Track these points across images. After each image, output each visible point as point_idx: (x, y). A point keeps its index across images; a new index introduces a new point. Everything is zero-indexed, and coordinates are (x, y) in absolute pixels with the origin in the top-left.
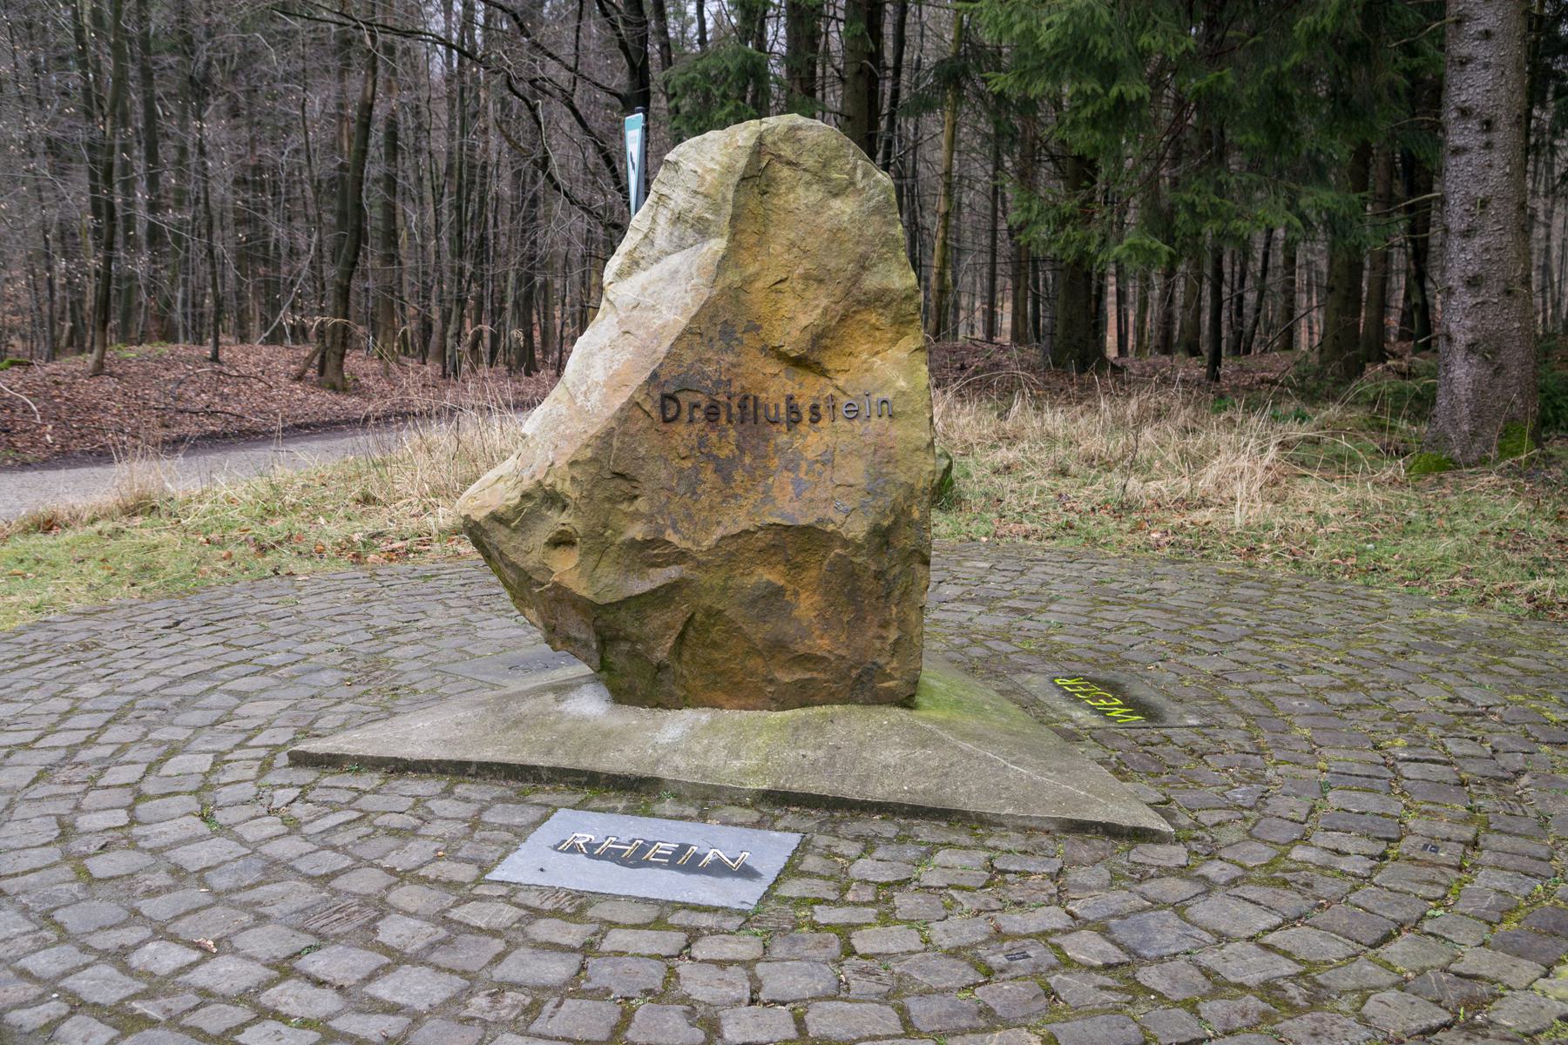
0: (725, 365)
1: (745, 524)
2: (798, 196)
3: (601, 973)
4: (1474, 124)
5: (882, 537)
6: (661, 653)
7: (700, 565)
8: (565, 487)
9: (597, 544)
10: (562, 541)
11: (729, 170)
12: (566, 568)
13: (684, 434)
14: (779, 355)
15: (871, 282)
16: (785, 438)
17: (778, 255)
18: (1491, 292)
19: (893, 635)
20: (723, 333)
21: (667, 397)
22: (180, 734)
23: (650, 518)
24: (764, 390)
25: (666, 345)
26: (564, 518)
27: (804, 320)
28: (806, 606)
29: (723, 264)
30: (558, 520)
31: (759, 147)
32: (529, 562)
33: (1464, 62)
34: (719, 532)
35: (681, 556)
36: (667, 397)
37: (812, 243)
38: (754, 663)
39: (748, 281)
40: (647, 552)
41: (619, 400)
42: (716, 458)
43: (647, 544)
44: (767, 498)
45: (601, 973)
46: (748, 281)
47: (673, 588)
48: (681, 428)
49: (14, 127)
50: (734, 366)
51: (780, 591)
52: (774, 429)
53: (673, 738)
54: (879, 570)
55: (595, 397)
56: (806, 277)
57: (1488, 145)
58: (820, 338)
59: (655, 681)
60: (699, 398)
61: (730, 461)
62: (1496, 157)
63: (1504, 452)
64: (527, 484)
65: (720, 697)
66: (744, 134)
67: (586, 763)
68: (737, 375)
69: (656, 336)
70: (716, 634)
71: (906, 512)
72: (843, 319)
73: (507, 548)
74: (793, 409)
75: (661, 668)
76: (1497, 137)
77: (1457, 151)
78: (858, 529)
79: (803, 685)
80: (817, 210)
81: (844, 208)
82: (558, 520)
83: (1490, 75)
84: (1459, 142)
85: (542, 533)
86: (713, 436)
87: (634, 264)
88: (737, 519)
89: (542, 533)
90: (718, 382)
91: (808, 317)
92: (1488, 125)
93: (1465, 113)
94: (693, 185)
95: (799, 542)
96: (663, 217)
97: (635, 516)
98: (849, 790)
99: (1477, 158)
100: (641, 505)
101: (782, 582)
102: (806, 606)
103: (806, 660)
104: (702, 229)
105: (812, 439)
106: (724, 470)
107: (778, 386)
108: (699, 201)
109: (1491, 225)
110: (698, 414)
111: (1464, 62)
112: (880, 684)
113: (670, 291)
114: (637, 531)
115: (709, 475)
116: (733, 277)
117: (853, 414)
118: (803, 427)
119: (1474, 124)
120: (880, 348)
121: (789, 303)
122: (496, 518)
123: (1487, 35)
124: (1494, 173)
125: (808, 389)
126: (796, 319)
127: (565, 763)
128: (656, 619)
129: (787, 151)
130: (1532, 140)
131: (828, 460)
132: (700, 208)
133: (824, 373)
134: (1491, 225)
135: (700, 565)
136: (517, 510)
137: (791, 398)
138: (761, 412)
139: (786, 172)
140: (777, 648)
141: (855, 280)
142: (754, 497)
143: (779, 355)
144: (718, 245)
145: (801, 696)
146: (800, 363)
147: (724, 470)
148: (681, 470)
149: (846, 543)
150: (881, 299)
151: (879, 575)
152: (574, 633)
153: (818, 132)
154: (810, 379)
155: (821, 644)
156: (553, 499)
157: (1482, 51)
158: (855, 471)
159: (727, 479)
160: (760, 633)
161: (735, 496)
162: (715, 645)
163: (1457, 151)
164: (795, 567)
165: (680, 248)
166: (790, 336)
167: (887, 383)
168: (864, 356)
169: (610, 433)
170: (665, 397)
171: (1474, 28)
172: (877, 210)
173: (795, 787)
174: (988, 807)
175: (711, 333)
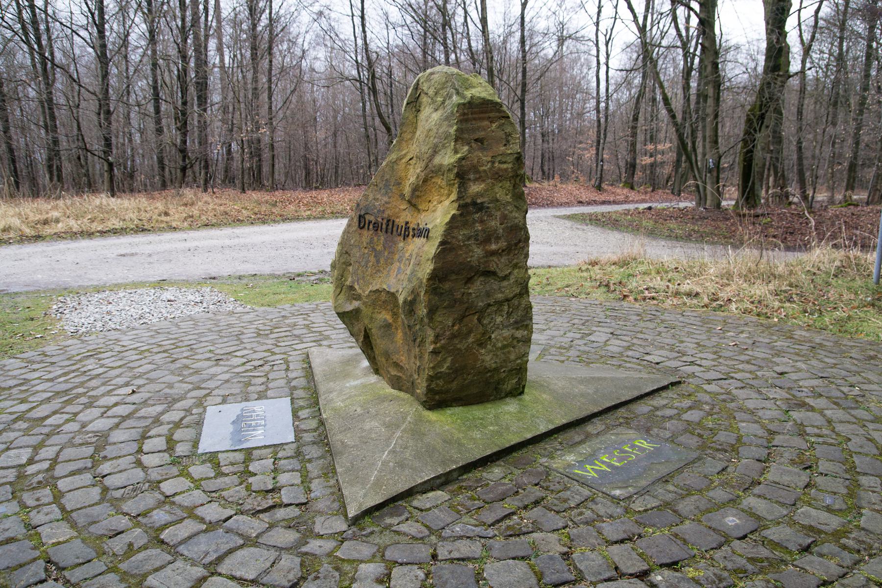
0: (383, 202)
3: (46, 494)
13: (367, 234)
15: (437, 160)
16: (401, 244)
20: (385, 185)
22: (659, 490)
24: (398, 217)
42: (375, 250)
45: (46, 494)
49: (541, 19)
50: (386, 203)
52: (399, 238)
60: (372, 218)
61: (380, 252)
68: (387, 208)
72: (425, 181)
74: (407, 229)
86: (375, 238)
90: (379, 211)
101: (391, 321)
110: (371, 227)
115: (372, 259)
118: (410, 239)
120: (443, 199)
137: (407, 223)
138: (395, 229)
141: (431, 158)
148: (364, 254)
159: (378, 261)
161: (379, 271)
168: (435, 203)
170: (360, 216)
175: (381, 185)
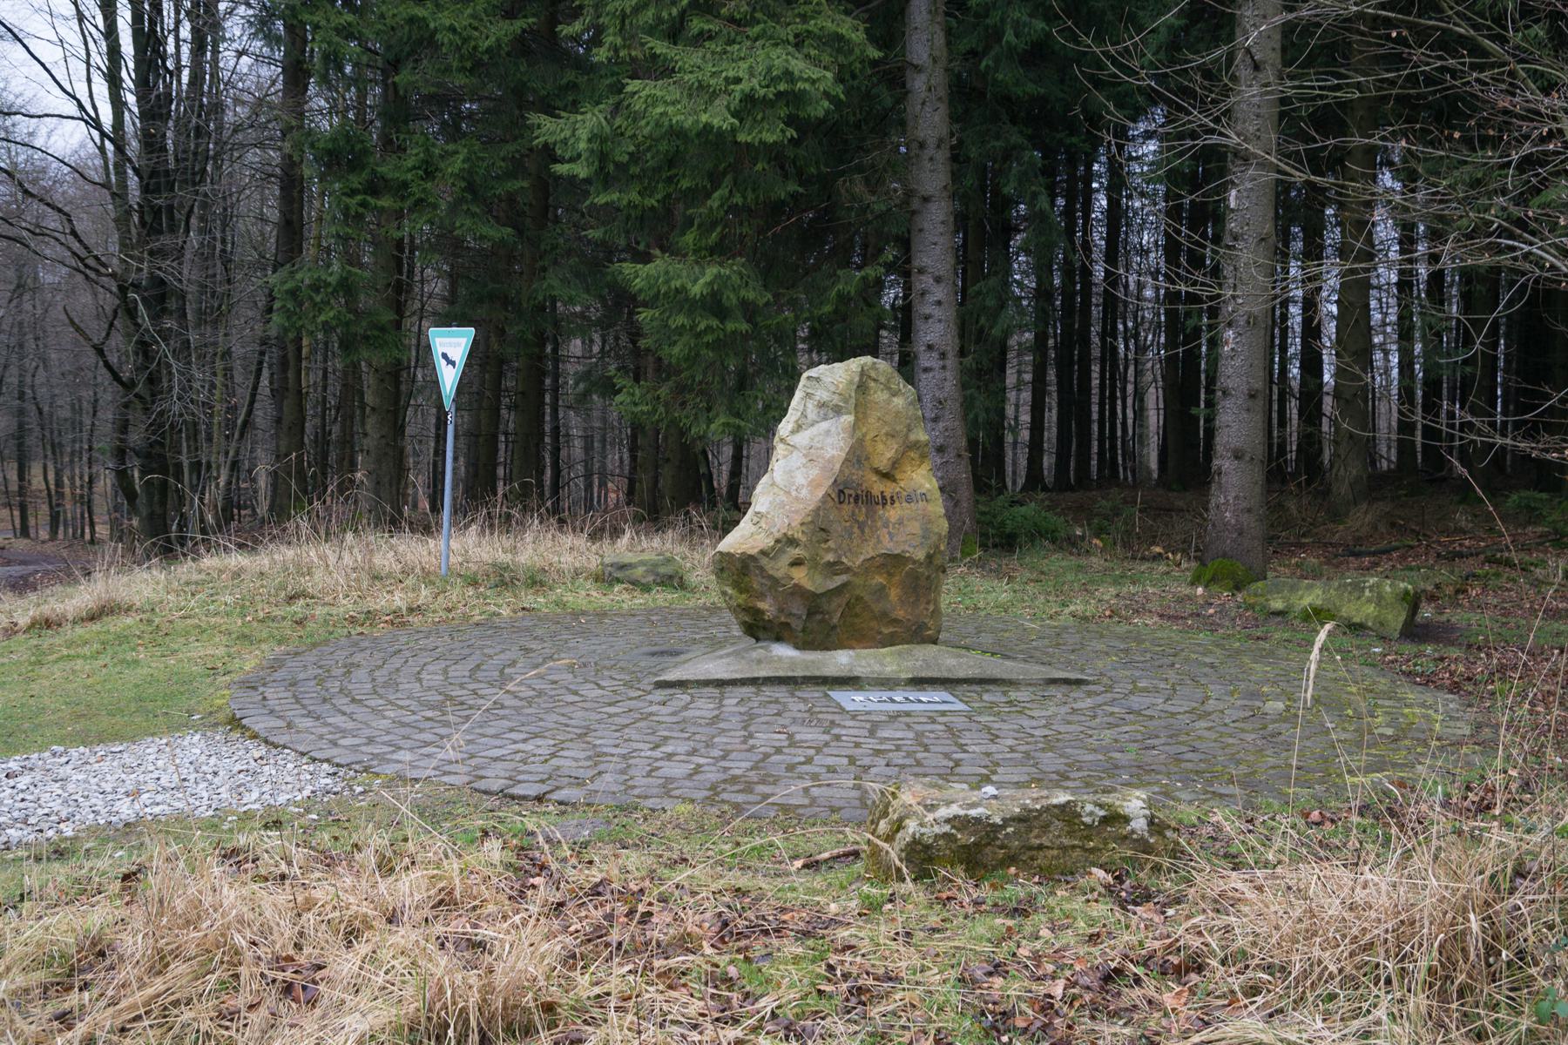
1: (872, 554)
2: (880, 396)
4: (935, 355)
5: (929, 557)
6: (835, 621)
7: (855, 574)
8: (798, 535)
9: (814, 564)
10: (797, 563)
11: (851, 382)
12: (800, 576)
13: (847, 508)
14: (877, 472)
15: (913, 437)
17: (873, 425)
18: (950, 455)
19: (931, 608)
21: (841, 492)
23: (836, 551)
25: (838, 466)
26: (797, 551)
27: (889, 455)
28: (894, 594)
29: (855, 427)
30: (796, 552)
31: (862, 373)
32: (778, 574)
33: (927, 317)
34: (862, 558)
35: (848, 570)
36: (841, 492)
37: (888, 418)
38: (874, 624)
39: (864, 435)
40: (834, 568)
41: (820, 493)
43: (835, 563)
44: (879, 542)
46: (864, 435)
47: (844, 585)
48: (845, 506)
51: (883, 588)
53: (841, 660)
54: (920, 580)
55: (804, 492)
56: (887, 434)
57: (944, 367)
58: (896, 463)
59: (828, 635)
62: (948, 374)
63: (965, 554)
64: (778, 535)
65: (854, 643)
66: (855, 364)
67: (818, 673)
69: (829, 461)
70: (858, 609)
71: (937, 547)
73: (767, 568)
74: (884, 498)
75: (834, 628)
76: (949, 363)
77: (926, 370)
78: (920, 555)
79: (892, 635)
80: (888, 402)
81: (899, 402)
82: (796, 552)
83: (941, 326)
84: (927, 364)
85: (785, 560)
87: (798, 428)
88: (868, 551)
89: (785, 560)
91: (889, 454)
92: (943, 356)
93: (930, 347)
94: (833, 389)
95: (893, 562)
96: (811, 405)
97: (829, 550)
98: (946, 675)
99: (938, 374)
100: (831, 544)
102: (894, 594)
103: (896, 621)
104: (838, 411)
105: (892, 512)
106: (861, 527)
107: (878, 487)
108: (836, 397)
109: (948, 415)
111: (927, 317)
112: (920, 634)
113: (829, 440)
114: (830, 557)
115: (856, 530)
116: (859, 434)
117: (909, 500)
118: (888, 507)
119: (935, 355)
121: (880, 447)
122: (763, 553)
123: (939, 303)
124: (947, 384)
125: (889, 488)
126: (884, 454)
127: (808, 674)
128: (836, 602)
129: (873, 374)
130: (549, 349)
131: (901, 522)
132: (836, 400)
133: (895, 481)
134: (948, 415)
135: (855, 574)
136: (773, 548)
139: (872, 384)
140: (885, 617)
141: (907, 436)
142: (874, 541)
143: (877, 472)
144: (848, 419)
145: (890, 641)
146: (887, 476)
147: (861, 527)
149: (914, 562)
150: (915, 445)
151: (928, 578)
152: (795, 611)
153: (883, 366)
154: (889, 483)
155: (900, 614)
156: (792, 542)
157: (937, 312)
158: (915, 527)
160: (877, 608)
162: (857, 615)
163: (926, 370)
164: (890, 575)
165: (825, 419)
166: (883, 462)
167: (921, 486)
169: (818, 508)
171: (932, 298)
172: (911, 403)
173: (923, 675)
174: (1014, 676)
